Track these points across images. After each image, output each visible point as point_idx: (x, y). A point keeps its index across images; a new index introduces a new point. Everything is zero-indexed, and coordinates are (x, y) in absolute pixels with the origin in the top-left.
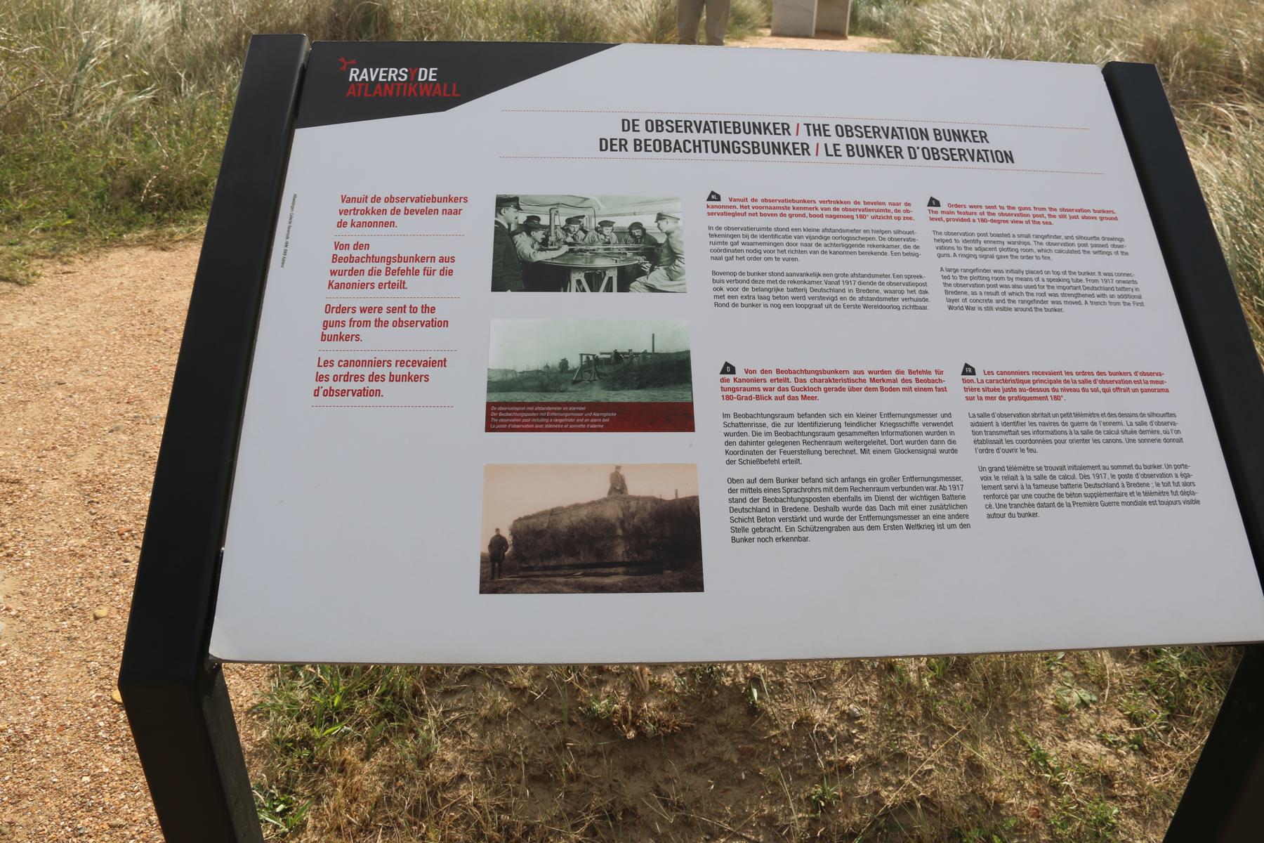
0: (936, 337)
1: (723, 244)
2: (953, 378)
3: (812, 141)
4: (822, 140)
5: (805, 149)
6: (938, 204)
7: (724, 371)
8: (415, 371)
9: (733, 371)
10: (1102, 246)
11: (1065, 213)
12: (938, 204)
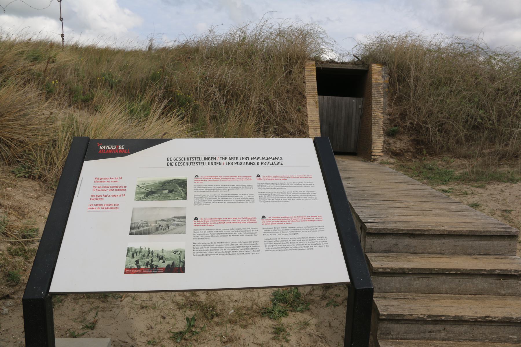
0: (257, 209)
1: (197, 189)
2: (259, 219)
3: (222, 161)
4: (225, 161)
5: (220, 164)
6: (260, 176)
7: (195, 219)
8: (114, 207)
9: (197, 219)
10: (309, 185)
11: (292, 177)
12: (260, 176)
